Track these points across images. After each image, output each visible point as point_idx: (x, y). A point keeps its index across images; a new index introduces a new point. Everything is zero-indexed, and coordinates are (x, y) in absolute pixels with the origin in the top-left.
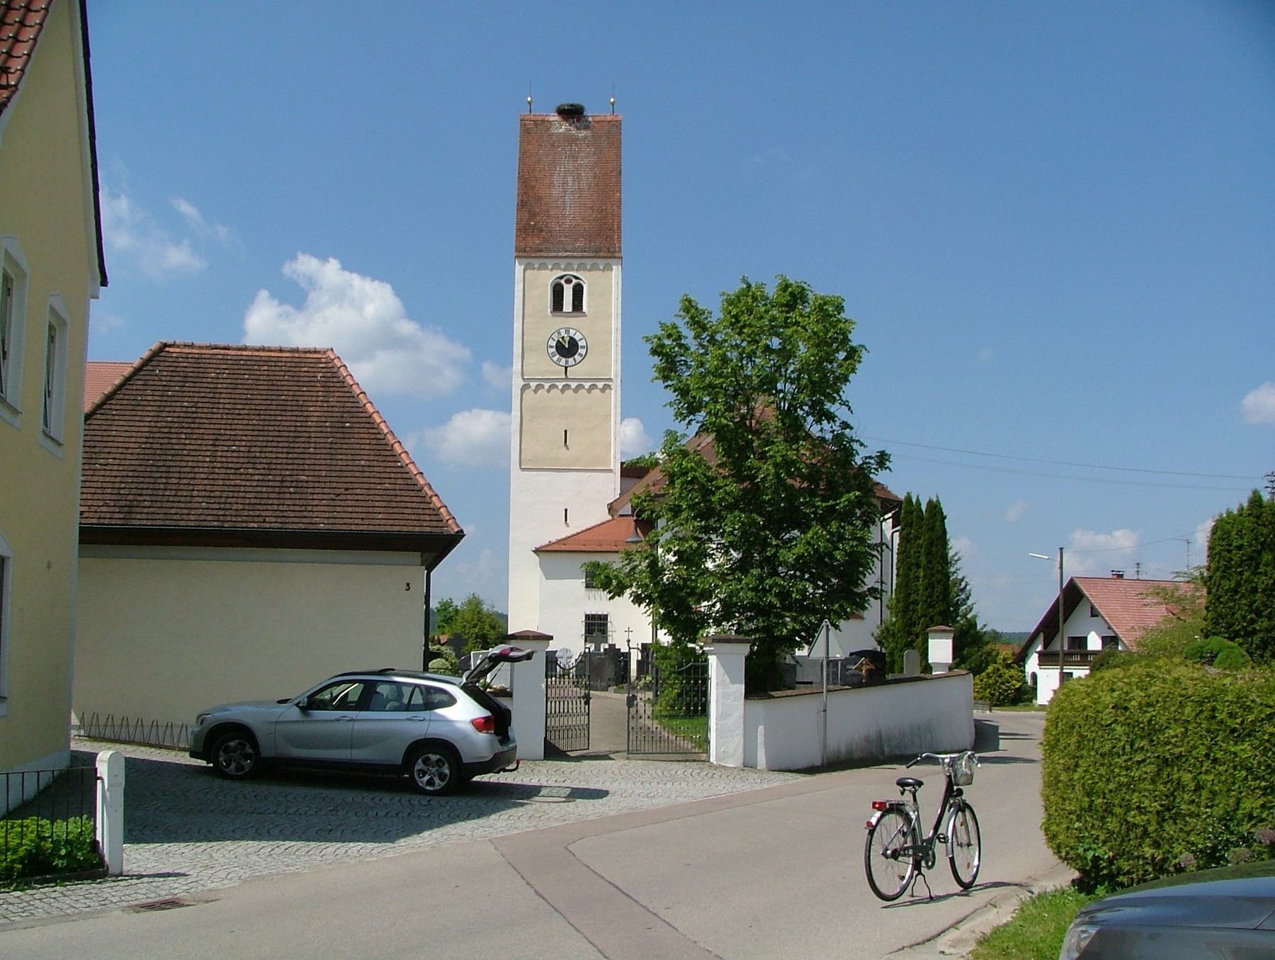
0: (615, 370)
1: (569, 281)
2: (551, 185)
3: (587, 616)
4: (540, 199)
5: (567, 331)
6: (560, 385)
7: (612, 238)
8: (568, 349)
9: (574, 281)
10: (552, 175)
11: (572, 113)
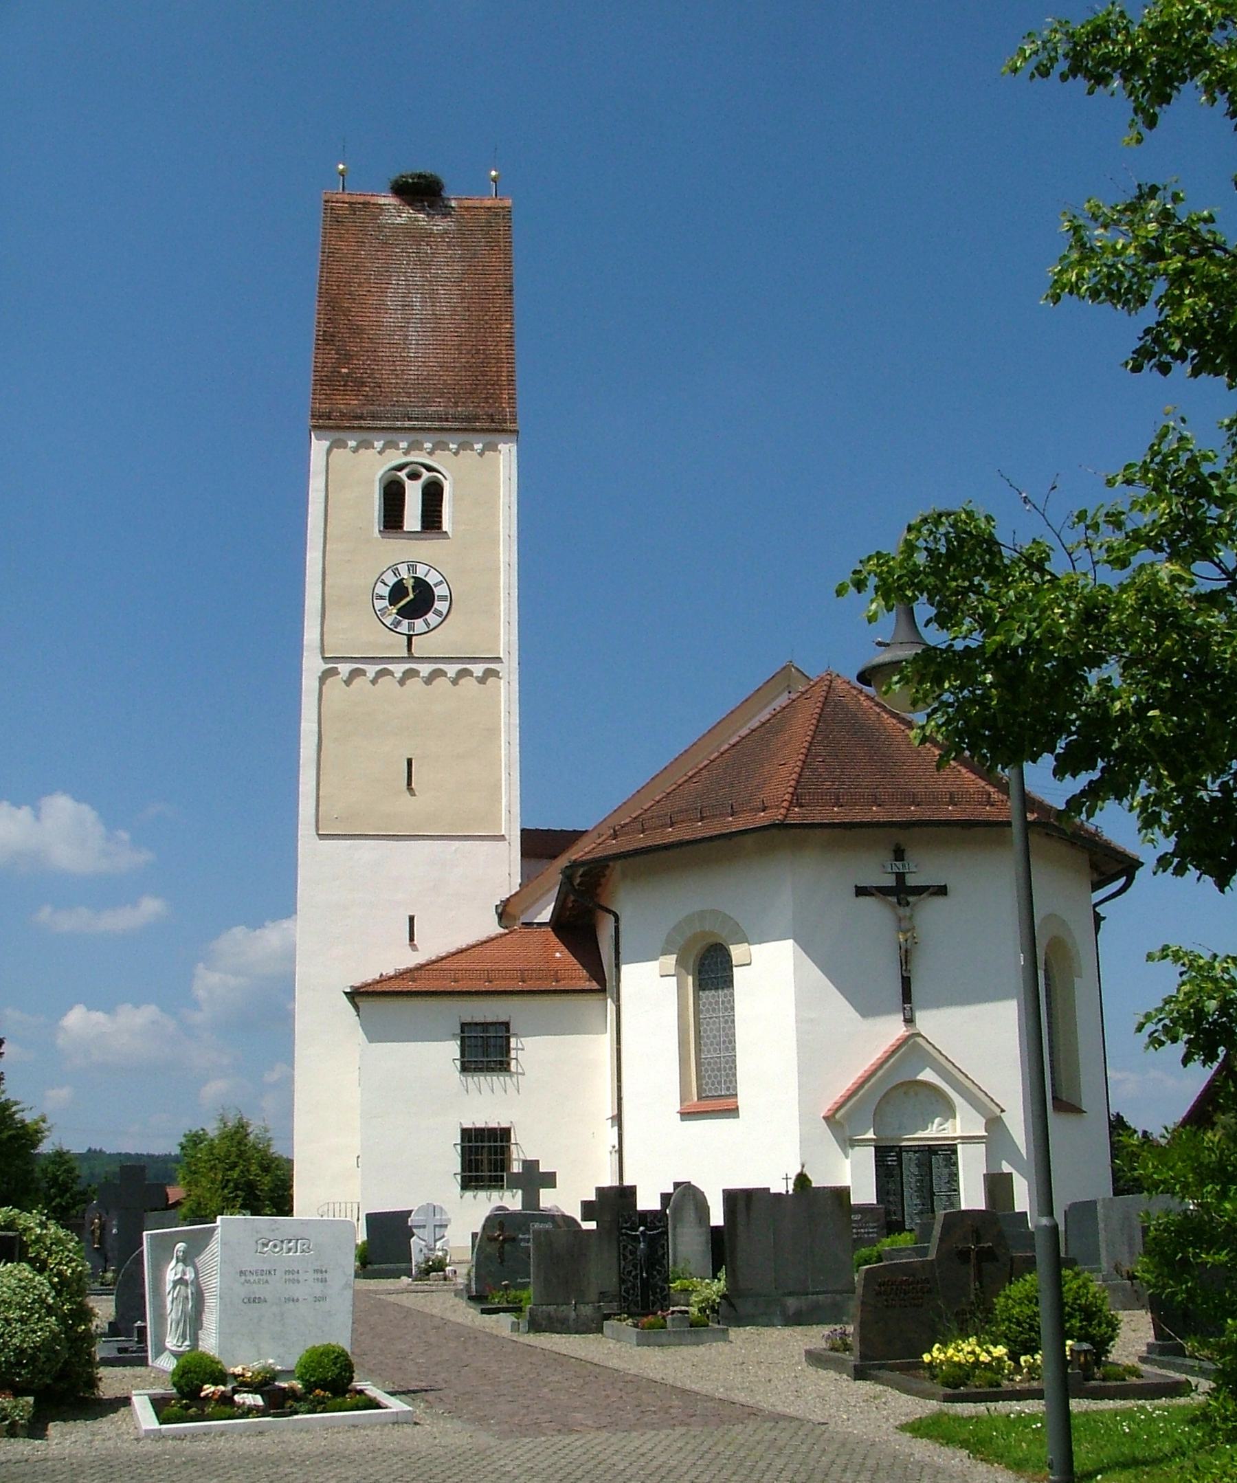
0: (506, 639)
1: (414, 476)
2: (380, 308)
3: (466, 1134)
4: (357, 331)
5: (412, 568)
6: (398, 669)
8: (414, 600)
9: (426, 475)
11: (421, 191)
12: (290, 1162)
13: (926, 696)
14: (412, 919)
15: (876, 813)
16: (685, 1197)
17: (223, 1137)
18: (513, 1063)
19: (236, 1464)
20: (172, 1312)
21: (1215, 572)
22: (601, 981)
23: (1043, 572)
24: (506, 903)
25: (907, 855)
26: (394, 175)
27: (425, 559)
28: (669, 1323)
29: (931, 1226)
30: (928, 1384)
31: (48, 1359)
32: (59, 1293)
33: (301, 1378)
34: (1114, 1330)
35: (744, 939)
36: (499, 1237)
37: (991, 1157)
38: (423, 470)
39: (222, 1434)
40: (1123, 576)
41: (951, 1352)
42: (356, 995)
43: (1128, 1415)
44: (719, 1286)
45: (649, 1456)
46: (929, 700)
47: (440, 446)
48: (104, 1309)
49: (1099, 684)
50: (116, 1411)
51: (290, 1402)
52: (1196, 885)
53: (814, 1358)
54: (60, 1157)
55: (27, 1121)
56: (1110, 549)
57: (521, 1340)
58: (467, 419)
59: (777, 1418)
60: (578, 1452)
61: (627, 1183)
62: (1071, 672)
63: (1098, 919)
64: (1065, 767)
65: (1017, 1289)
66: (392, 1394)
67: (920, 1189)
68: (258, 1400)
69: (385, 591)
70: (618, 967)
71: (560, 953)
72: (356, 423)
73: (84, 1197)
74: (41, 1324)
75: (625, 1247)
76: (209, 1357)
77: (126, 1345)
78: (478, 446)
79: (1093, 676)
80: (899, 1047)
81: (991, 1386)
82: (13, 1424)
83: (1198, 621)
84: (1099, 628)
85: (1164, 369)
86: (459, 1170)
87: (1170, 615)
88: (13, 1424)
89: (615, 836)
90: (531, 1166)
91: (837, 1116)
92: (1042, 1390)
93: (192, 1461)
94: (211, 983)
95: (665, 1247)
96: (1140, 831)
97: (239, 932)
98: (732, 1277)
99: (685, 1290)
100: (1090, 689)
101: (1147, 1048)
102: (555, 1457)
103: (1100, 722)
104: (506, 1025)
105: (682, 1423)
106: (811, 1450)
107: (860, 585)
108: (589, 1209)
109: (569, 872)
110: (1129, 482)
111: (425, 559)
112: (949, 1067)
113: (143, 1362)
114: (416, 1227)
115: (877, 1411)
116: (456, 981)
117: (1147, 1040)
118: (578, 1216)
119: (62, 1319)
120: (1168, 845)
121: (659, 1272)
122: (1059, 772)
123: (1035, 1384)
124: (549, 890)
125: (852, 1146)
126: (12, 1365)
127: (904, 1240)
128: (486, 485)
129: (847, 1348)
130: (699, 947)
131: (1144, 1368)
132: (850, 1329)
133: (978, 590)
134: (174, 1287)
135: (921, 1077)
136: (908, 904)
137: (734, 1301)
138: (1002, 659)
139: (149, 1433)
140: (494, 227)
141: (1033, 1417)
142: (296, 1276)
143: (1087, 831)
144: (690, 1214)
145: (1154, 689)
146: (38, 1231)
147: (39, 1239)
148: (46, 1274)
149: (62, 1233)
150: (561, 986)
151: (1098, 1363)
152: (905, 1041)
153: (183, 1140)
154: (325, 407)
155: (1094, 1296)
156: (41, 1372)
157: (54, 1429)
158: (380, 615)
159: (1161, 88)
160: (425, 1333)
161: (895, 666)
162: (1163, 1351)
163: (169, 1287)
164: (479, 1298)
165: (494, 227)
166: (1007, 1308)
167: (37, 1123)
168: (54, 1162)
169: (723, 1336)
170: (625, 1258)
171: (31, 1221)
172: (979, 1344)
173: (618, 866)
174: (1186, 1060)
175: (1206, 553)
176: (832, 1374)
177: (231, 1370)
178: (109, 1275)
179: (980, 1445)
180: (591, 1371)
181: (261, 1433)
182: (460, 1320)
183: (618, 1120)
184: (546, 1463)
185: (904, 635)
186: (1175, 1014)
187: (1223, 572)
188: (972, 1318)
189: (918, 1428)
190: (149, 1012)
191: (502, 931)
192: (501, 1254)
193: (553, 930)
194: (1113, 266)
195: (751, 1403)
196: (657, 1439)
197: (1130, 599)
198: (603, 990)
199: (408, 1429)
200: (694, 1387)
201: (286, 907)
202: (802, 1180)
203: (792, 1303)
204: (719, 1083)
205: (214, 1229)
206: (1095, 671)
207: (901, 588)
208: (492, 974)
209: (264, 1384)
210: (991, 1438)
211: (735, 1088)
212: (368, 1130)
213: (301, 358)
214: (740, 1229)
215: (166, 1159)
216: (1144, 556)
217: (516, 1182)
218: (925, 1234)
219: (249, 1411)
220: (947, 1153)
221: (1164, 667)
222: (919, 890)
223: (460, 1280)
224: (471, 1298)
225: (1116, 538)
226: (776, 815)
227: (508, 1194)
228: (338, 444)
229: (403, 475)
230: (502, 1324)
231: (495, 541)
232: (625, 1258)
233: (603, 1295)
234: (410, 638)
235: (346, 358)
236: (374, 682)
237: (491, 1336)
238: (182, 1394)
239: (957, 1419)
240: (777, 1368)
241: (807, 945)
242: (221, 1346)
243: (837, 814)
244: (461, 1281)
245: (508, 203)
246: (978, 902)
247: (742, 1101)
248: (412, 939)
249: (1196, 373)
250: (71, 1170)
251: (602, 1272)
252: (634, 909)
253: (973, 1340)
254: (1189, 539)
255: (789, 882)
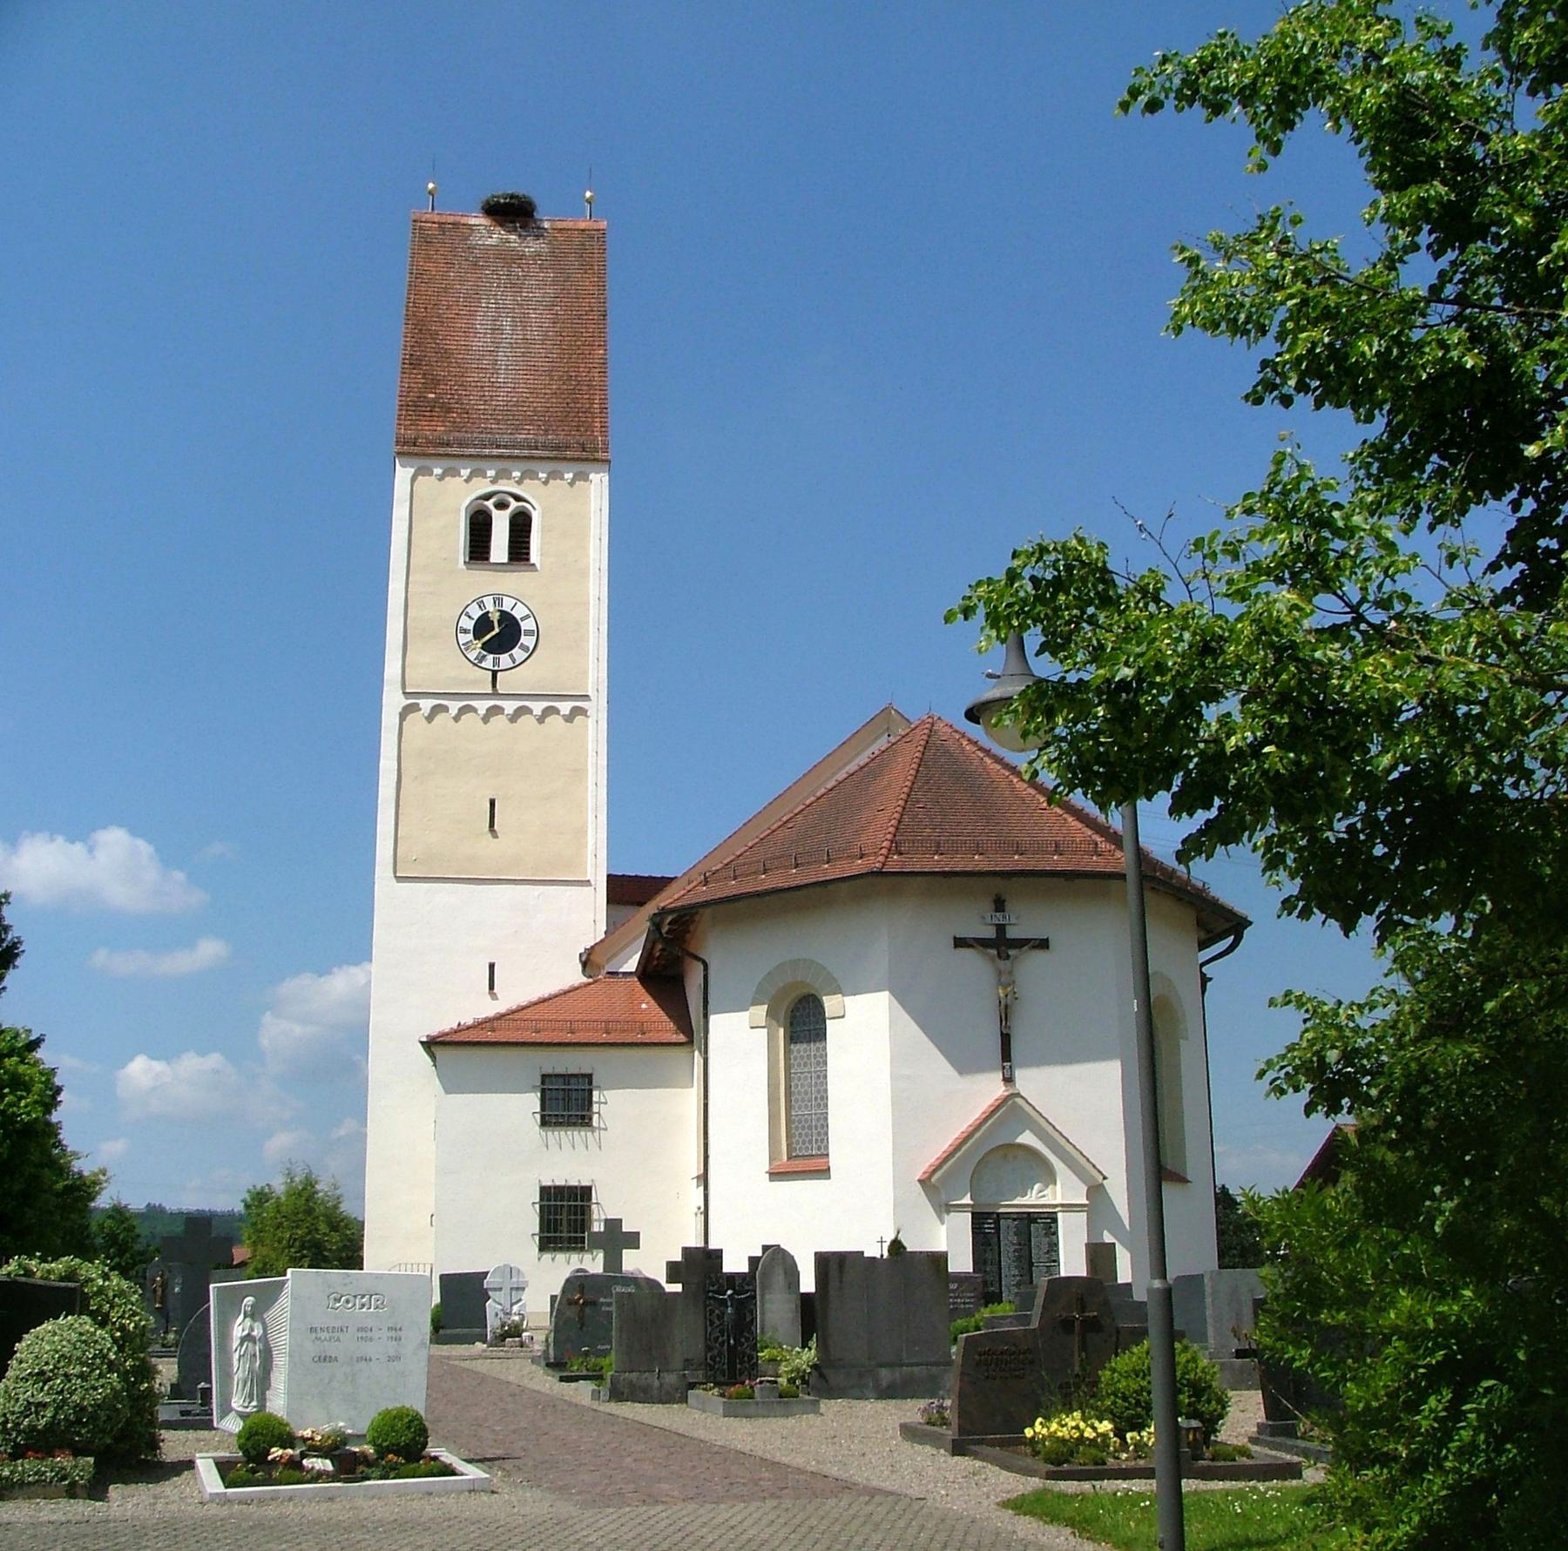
0: (595, 677)
1: (501, 506)
2: (469, 331)
3: (545, 1191)
4: (446, 354)
5: (498, 600)
6: (482, 706)
7: (590, 428)
8: (499, 634)
9: (514, 504)
10: (472, 314)
11: (512, 212)
12: (363, 1223)
13: (1037, 729)
14: (492, 966)
15: (978, 862)
16: (775, 1260)
17: (289, 1194)
18: (595, 1117)
19: (306, 1530)
20: (240, 1370)
21: (1339, 605)
22: (690, 1033)
23: (1157, 600)
24: (590, 951)
25: (1008, 905)
26: (485, 195)
27: (512, 591)
28: (757, 1393)
29: (1032, 1297)
30: (1029, 1460)
31: (109, 1418)
32: (121, 1349)
33: (373, 1443)
34: (1224, 1408)
35: (837, 990)
36: (579, 1300)
37: (1092, 1226)
38: (511, 500)
39: (290, 1499)
40: (1240, 608)
41: (1054, 1426)
42: (432, 1045)
43: (1241, 1496)
44: (809, 1356)
45: (740, 1529)
46: (1041, 733)
47: (528, 475)
48: (167, 1371)
49: (1219, 721)
50: (178, 1475)
51: (361, 1468)
52: (1322, 929)
53: (910, 1432)
54: (118, 1213)
55: (86, 1174)
56: (1230, 582)
57: (601, 1408)
58: (557, 448)
59: (873, 1492)
60: (664, 1524)
61: (712, 1246)
62: (1187, 705)
63: (1205, 980)
64: (1180, 807)
65: (1123, 1362)
66: (469, 1461)
67: (1019, 1259)
68: (327, 1465)
69: (470, 625)
70: (706, 1016)
71: (647, 1004)
72: (441, 450)
73: (144, 1257)
74: (102, 1381)
75: (712, 1312)
76: (276, 1418)
77: (189, 1408)
78: (569, 476)
79: (1211, 712)
80: (998, 1108)
81: (1096, 1464)
82: (73, 1484)
83: (1318, 654)
84: (1215, 661)
85: (1286, 401)
86: (537, 1230)
87: (1286, 649)
88: (73, 1484)
89: (706, 882)
90: (613, 1225)
91: (933, 1179)
92: (1153, 1470)
93: (260, 1525)
94: (280, 1033)
95: (752, 1312)
96: (1264, 871)
97: (306, 979)
98: (823, 1347)
99: (773, 1360)
100: (1209, 725)
101: (1268, 1095)
102: (640, 1529)
103: (1216, 759)
104: (590, 1076)
105: (772, 1495)
106: (909, 1525)
107: (967, 612)
108: (674, 1271)
109: (657, 919)
110: (1249, 511)
111: (512, 591)
112: (1050, 1129)
113: (208, 1425)
114: (495, 1290)
115: (979, 1487)
116: (538, 1031)
117: (1268, 1087)
118: (662, 1280)
119: (124, 1376)
120: (1293, 887)
121: (747, 1339)
122: (1175, 810)
123: (1141, 1462)
124: (635, 939)
125: (948, 1212)
126: (72, 1423)
127: (1004, 1309)
128: (576, 516)
129: (944, 1422)
130: (786, 1003)
131: (1254, 1448)
132: (948, 1403)
133: (1092, 621)
134: (241, 1344)
135: (1020, 1140)
136: (1008, 957)
137: (825, 1371)
138: (1112, 691)
139: (215, 1497)
140: (587, 251)
141: (1141, 1496)
142: (369, 1334)
143: (1193, 886)
144: (779, 1279)
145: (1271, 725)
146: (100, 1282)
147: (101, 1291)
148: (108, 1327)
149: (125, 1284)
150: (646, 1038)
151: (1207, 1442)
152: (1006, 1099)
153: (247, 1197)
154: (411, 434)
155: (1203, 1371)
156: (103, 1431)
157: (115, 1491)
158: (464, 649)
159: (1286, 110)
160: (501, 1400)
161: (1007, 700)
162: (1274, 1432)
163: (236, 1343)
164: (557, 1364)
165: (587, 251)
166: (1111, 1382)
167: (96, 1174)
168: (110, 1217)
169: (814, 1408)
170: (712, 1323)
171: (92, 1271)
172: (1084, 1419)
173: (708, 911)
174: (1309, 1109)
175: (1327, 584)
176: (928, 1449)
177: (300, 1433)
178: (171, 1336)
179: (1083, 1523)
180: (676, 1442)
181: (331, 1499)
182: (537, 1388)
183: (704, 1179)
184: (631, 1535)
185: (1015, 667)
186: (1298, 1062)
187: (1347, 605)
188: (1076, 1392)
189: (1018, 1505)
190: (214, 1060)
191: (585, 980)
192: (581, 1318)
193: (640, 979)
194: (1233, 296)
195: (845, 1476)
196: (745, 1513)
197: (1247, 629)
198: (690, 1042)
199: (485, 1498)
200: (785, 1460)
201: (361, 951)
202: (896, 1246)
203: (885, 1375)
204: (810, 1142)
205: (284, 1283)
206: (1213, 706)
207: (1008, 618)
208: (575, 1025)
209: (334, 1448)
210: (1098, 1517)
211: (827, 1147)
212: (443, 1187)
213: (385, 382)
214: (833, 1293)
215: (230, 1217)
216: (1266, 585)
217: (599, 1242)
218: (1026, 1302)
219: (318, 1476)
220: (1048, 1221)
221: (1284, 701)
222: (1020, 943)
223: (537, 1347)
224: (548, 1365)
225: (1236, 570)
226: (875, 863)
227: (588, 1257)
228: (422, 471)
229: (490, 504)
230: (582, 1392)
231: (584, 574)
232: (712, 1323)
233: (688, 1363)
234: (495, 674)
235: (433, 383)
236: (456, 719)
237: (570, 1404)
238: (249, 1458)
239: (1062, 1495)
240: (871, 1441)
241: (903, 996)
242: (290, 1409)
243: (937, 862)
244: (538, 1347)
245: (603, 224)
246: (1087, 956)
247: (834, 1161)
248: (491, 987)
249: (1319, 404)
250: (131, 1228)
251: (687, 1338)
252: (725, 957)
253: (1077, 1414)
254: (1311, 570)
255: (883, 932)
